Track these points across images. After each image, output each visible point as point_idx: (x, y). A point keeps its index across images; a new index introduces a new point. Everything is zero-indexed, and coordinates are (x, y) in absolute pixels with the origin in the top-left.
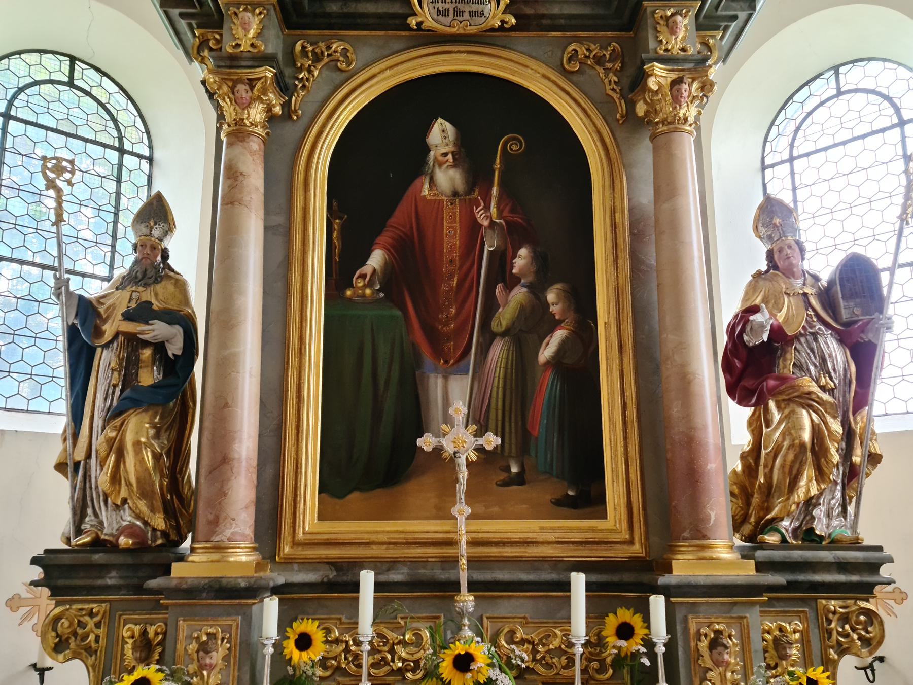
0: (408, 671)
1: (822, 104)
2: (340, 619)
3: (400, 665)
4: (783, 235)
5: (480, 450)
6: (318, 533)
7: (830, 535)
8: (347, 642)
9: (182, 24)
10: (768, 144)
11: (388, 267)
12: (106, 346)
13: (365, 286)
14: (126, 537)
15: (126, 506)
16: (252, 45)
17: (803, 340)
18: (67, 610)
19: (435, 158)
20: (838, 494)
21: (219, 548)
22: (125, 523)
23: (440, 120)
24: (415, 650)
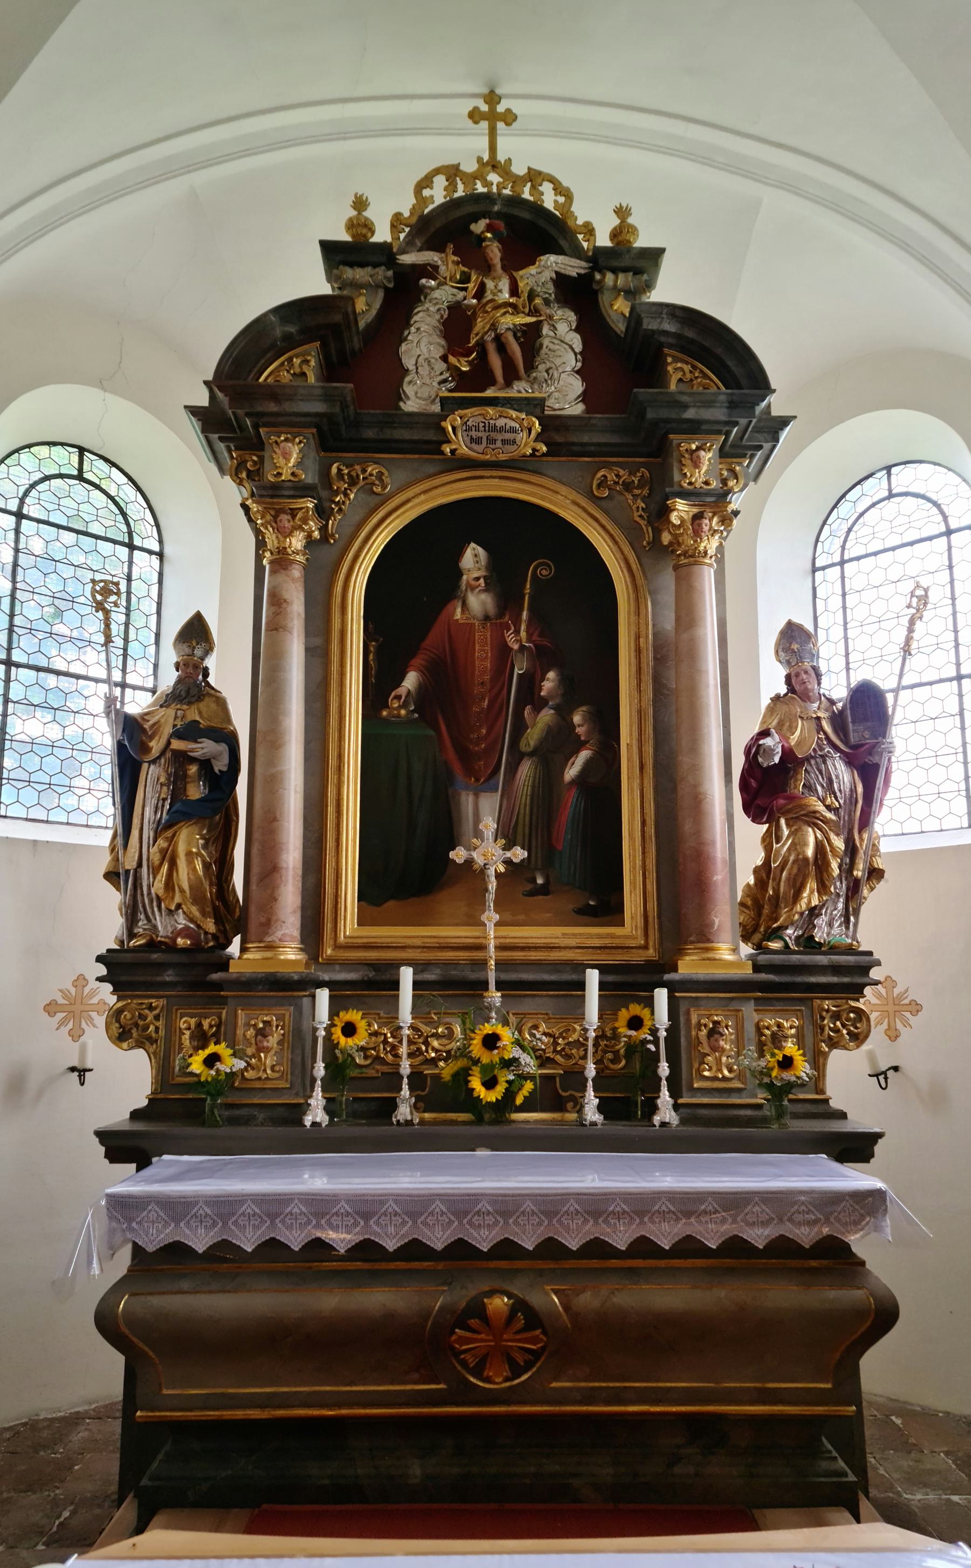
0: (441, 1060)
1: (873, 505)
2: (379, 1014)
3: (433, 1055)
4: (801, 660)
5: (508, 862)
6: (357, 937)
7: (829, 942)
8: (385, 1035)
9: (221, 447)
10: (820, 544)
11: (421, 688)
12: (154, 762)
13: (400, 707)
14: (182, 938)
15: (180, 911)
16: (293, 474)
17: (813, 762)
18: (129, 1004)
19: (468, 582)
20: (840, 906)
21: (271, 947)
22: (180, 927)
23: (473, 545)
24: (447, 1042)
